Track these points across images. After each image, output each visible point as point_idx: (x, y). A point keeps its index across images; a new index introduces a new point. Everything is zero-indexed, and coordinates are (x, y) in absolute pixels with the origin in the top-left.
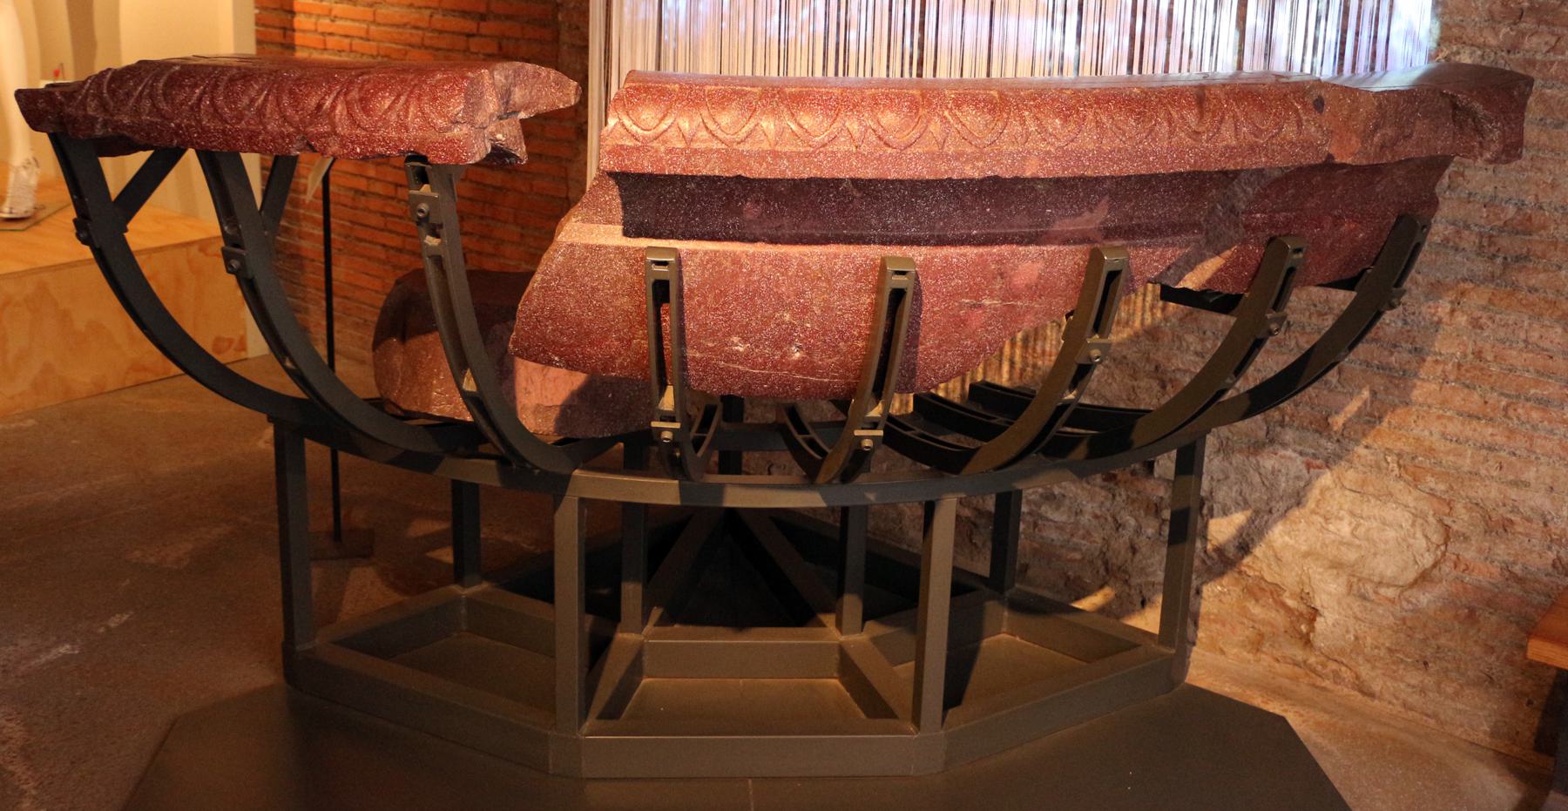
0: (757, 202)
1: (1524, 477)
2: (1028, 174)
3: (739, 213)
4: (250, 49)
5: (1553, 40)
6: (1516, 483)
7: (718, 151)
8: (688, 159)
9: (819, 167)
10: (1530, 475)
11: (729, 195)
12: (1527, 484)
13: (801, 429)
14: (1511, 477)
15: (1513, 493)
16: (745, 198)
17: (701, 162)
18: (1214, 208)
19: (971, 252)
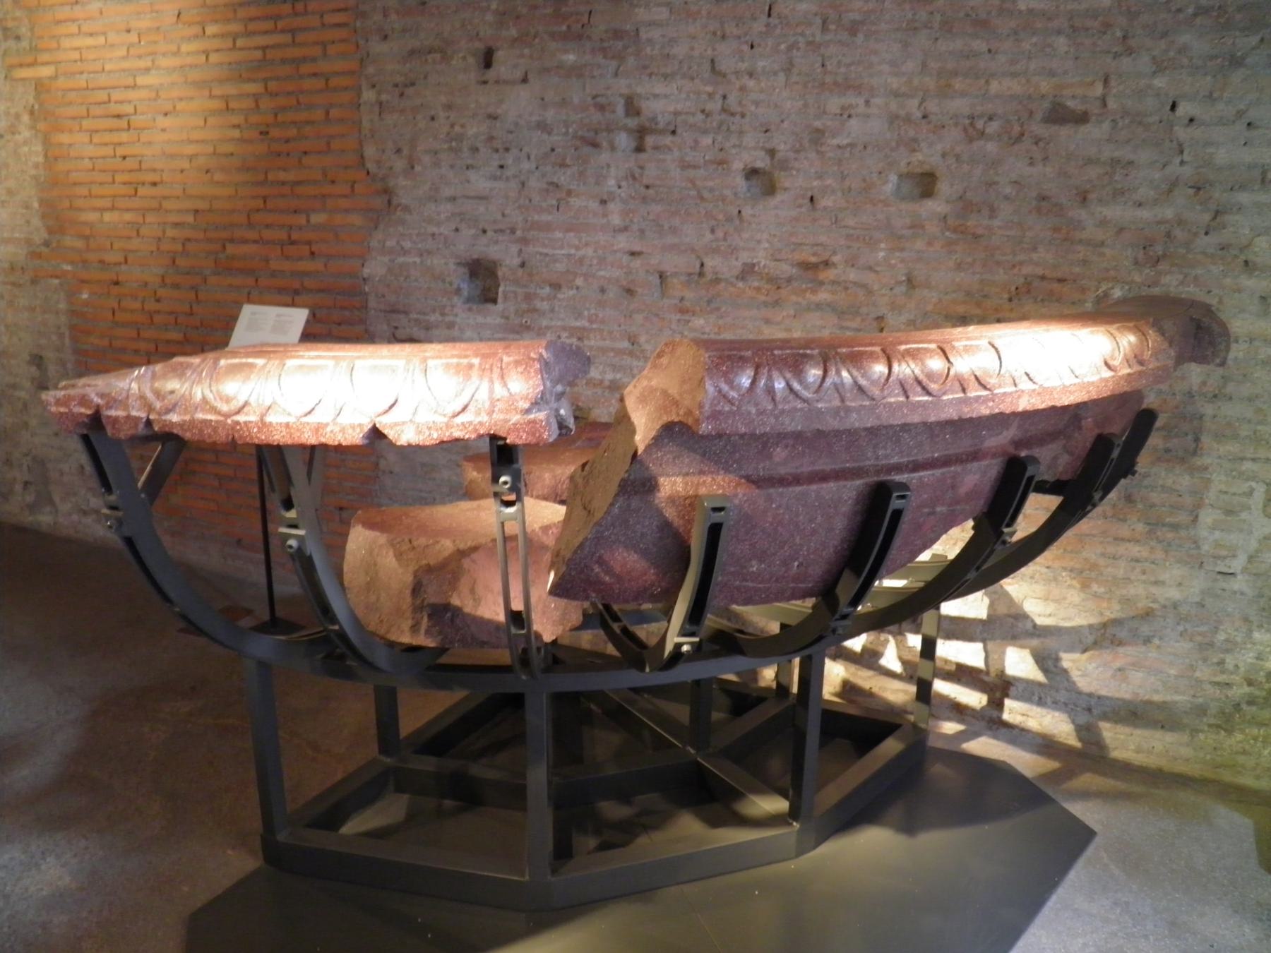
0: (786, 447)
1: (1161, 579)
2: (1020, 409)
3: (770, 457)
4: (540, 349)
5: (1181, 277)
6: (1156, 583)
7: (801, 409)
8: (777, 418)
9: (878, 417)
10: (1165, 576)
11: (765, 445)
12: (1163, 583)
13: (616, 619)
14: (1153, 579)
15: (1154, 590)
16: (777, 445)
17: (787, 421)
18: (929, 393)
19: (938, 472)
